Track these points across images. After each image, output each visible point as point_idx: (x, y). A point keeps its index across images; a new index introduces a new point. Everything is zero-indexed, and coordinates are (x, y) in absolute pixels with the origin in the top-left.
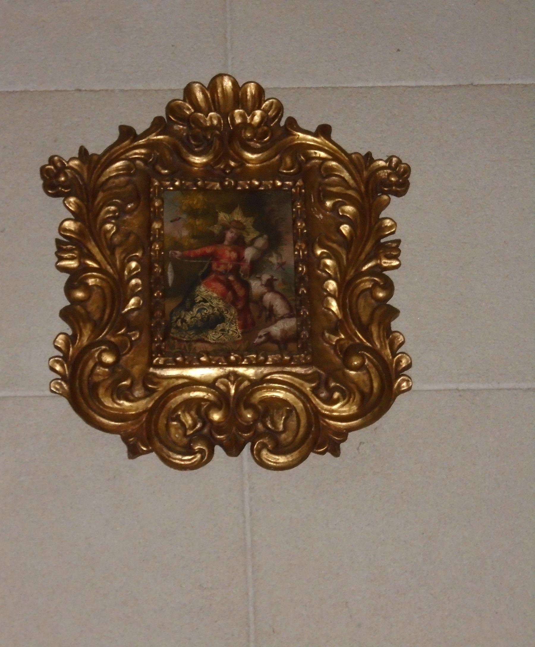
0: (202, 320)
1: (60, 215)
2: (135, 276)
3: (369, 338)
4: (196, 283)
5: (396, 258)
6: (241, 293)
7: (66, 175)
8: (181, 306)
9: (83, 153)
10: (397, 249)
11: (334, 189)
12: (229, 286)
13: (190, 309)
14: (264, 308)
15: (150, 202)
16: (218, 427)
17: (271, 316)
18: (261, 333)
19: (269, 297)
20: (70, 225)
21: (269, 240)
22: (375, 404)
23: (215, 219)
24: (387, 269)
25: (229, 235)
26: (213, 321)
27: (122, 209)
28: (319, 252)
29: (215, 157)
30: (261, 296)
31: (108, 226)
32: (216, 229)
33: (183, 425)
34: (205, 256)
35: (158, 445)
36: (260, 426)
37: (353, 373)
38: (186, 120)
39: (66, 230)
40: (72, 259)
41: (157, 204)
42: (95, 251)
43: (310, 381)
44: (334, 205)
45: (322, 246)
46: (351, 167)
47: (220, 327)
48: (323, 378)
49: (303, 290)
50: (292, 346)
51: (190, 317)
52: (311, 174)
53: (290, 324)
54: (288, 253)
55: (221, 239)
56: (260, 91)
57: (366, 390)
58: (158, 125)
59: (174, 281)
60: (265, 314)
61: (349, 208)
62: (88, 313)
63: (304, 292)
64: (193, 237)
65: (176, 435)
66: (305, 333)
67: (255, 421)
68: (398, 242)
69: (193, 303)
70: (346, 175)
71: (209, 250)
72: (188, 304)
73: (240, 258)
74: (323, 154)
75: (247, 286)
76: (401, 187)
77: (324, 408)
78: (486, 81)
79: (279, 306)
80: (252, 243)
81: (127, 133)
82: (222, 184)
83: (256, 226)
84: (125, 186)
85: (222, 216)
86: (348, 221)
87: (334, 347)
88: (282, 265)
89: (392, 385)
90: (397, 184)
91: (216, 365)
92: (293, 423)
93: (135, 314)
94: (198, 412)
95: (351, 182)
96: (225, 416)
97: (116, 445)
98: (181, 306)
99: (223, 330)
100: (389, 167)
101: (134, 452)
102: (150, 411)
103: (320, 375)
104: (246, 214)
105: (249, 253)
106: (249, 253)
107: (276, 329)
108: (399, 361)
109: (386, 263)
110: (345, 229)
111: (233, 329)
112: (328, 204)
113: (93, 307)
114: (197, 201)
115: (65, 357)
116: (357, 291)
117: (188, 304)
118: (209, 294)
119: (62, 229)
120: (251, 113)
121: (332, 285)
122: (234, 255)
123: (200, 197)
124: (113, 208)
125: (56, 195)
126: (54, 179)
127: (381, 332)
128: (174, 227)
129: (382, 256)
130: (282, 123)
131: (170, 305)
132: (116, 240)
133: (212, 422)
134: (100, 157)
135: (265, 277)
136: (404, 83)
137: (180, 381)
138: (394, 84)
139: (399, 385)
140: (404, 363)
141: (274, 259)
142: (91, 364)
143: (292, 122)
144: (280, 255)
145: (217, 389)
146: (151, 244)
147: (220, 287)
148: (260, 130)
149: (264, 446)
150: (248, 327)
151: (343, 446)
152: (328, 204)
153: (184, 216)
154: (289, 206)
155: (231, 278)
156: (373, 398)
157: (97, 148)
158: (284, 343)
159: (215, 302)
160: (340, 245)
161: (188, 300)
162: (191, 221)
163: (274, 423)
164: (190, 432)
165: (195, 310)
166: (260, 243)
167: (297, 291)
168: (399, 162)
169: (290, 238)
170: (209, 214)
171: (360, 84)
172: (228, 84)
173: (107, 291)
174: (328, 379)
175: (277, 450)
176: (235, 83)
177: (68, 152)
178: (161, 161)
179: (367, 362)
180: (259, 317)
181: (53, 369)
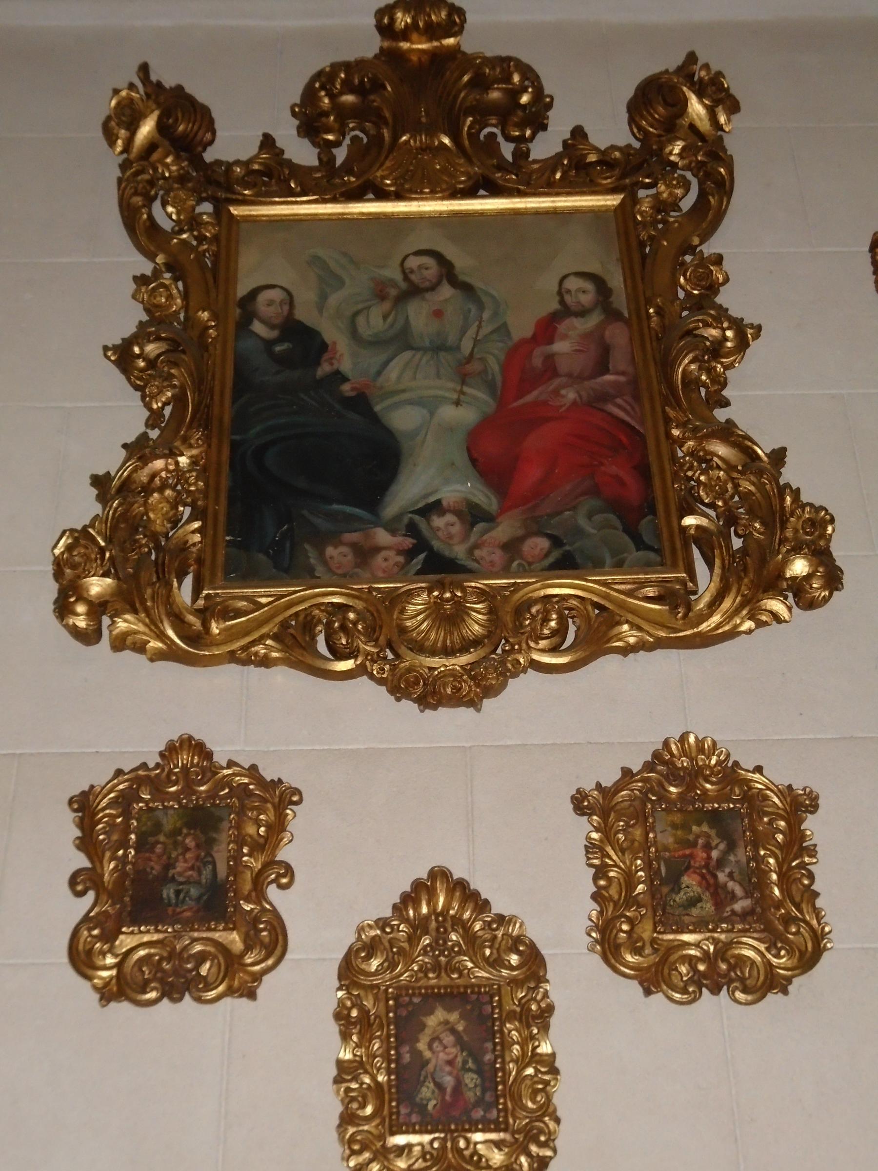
0: (687, 900)
1: (584, 829)
2: (641, 870)
3: (801, 912)
4: (681, 874)
5: (814, 856)
6: (712, 881)
7: (589, 801)
8: (672, 890)
9: (599, 786)
10: (814, 850)
11: (769, 810)
12: (703, 876)
13: (679, 892)
14: (728, 892)
15: (646, 819)
16: (703, 975)
17: (734, 898)
18: (728, 909)
19: (731, 884)
20: (595, 835)
21: (728, 845)
22: (808, 960)
23: (690, 831)
24: (808, 864)
25: (700, 841)
26: (694, 902)
27: (627, 824)
28: (762, 853)
29: (687, 788)
30: (726, 885)
31: (620, 836)
32: (691, 837)
33: (680, 974)
34: (685, 856)
35: (665, 987)
36: (732, 974)
37: (790, 936)
38: (664, 763)
39: (590, 838)
40: (597, 858)
41: (651, 820)
42: (612, 853)
43: (764, 943)
44: (770, 820)
45: (765, 849)
46: (779, 794)
47: (699, 905)
48: (773, 940)
49: (754, 880)
50: (749, 918)
51: (680, 897)
52: (754, 800)
53: (746, 903)
54: (741, 854)
55: (694, 845)
56: (714, 743)
57: (803, 949)
58: (649, 766)
59: (666, 873)
60: (729, 896)
61: (782, 823)
62: (610, 895)
63: (755, 881)
64: (678, 843)
65: (676, 980)
66: (759, 910)
67: (729, 970)
68: (815, 845)
69: (680, 889)
70: (776, 800)
71: (688, 852)
72: (676, 890)
73: (709, 857)
74: (760, 786)
75: (715, 877)
76: (814, 807)
77: (774, 961)
78: (860, 735)
79: (739, 891)
80: (716, 846)
81: (627, 773)
82: (693, 807)
83: (718, 835)
84: (628, 809)
85: (695, 828)
86: (781, 832)
87: (778, 919)
88: (737, 862)
89: (820, 945)
90: (811, 805)
91: (700, 932)
92: (755, 973)
93: (642, 896)
94: (690, 965)
95: (780, 804)
96: (708, 967)
97: (634, 988)
98: (672, 890)
99: (702, 907)
100: (805, 794)
101: (648, 992)
102: (657, 965)
103: (770, 939)
104: (711, 828)
105: (715, 854)
106: (715, 854)
107: (738, 906)
108: (823, 928)
109: (807, 859)
110: (780, 837)
111: (708, 907)
112: (766, 819)
113: (613, 892)
114: (677, 818)
115: (597, 926)
116: (791, 880)
117: (676, 890)
118: (690, 881)
119: (588, 838)
120: (709, 758)
121: (774, 877)
122: (705, 855)
123: (679, 815)
124: (622, 823)
125: (583, 814)
126: (580, 804)
127: (414, 196)
128: (664, 836)
129: (805, 855)
130: (730, 765)
131: (665, 890)
132: (624, 845)
133: (699, 971)
134: (610, 788)
135: (727, 870)
136: (806, 737)
137: (676, 943)
138: (800, 737)
139: (825, 945)
140: (827, 929)
141: (732, 858)
142: (615, 931)
143: (736, 763)
144: (736, 855)
145: (702, 948)
146: (649, 848)
147: (698, 878)
148: (715, 770)
149: (736, 988)
150: (719, 905)
151: (790, 988)
152: (766, 819)
153: (669, 829)
154: (739, 821)
155: (704, 871)
156: (808, 955)
157: (607, 783)
158: (744, 916)
159: (695, 888)
160: (776, 848)
161: (677, 888)
162: (674, 831)
163: (742, 972)
164: (685, 979)
165: (682, 893)
166: (722, 846)
167: (750, 880)
168: (811, 792)
169: (742, 844)
170: (685, 827)
171: (776, 737)
172: (692, 739)
173: (622, 881)
174: (774, 940)
175: (745, 991)
176: (696, 738)
177: (588, 786)
178: (651, 790)
179: (802, 929)
180: (726, 897)
181: (589, 935)
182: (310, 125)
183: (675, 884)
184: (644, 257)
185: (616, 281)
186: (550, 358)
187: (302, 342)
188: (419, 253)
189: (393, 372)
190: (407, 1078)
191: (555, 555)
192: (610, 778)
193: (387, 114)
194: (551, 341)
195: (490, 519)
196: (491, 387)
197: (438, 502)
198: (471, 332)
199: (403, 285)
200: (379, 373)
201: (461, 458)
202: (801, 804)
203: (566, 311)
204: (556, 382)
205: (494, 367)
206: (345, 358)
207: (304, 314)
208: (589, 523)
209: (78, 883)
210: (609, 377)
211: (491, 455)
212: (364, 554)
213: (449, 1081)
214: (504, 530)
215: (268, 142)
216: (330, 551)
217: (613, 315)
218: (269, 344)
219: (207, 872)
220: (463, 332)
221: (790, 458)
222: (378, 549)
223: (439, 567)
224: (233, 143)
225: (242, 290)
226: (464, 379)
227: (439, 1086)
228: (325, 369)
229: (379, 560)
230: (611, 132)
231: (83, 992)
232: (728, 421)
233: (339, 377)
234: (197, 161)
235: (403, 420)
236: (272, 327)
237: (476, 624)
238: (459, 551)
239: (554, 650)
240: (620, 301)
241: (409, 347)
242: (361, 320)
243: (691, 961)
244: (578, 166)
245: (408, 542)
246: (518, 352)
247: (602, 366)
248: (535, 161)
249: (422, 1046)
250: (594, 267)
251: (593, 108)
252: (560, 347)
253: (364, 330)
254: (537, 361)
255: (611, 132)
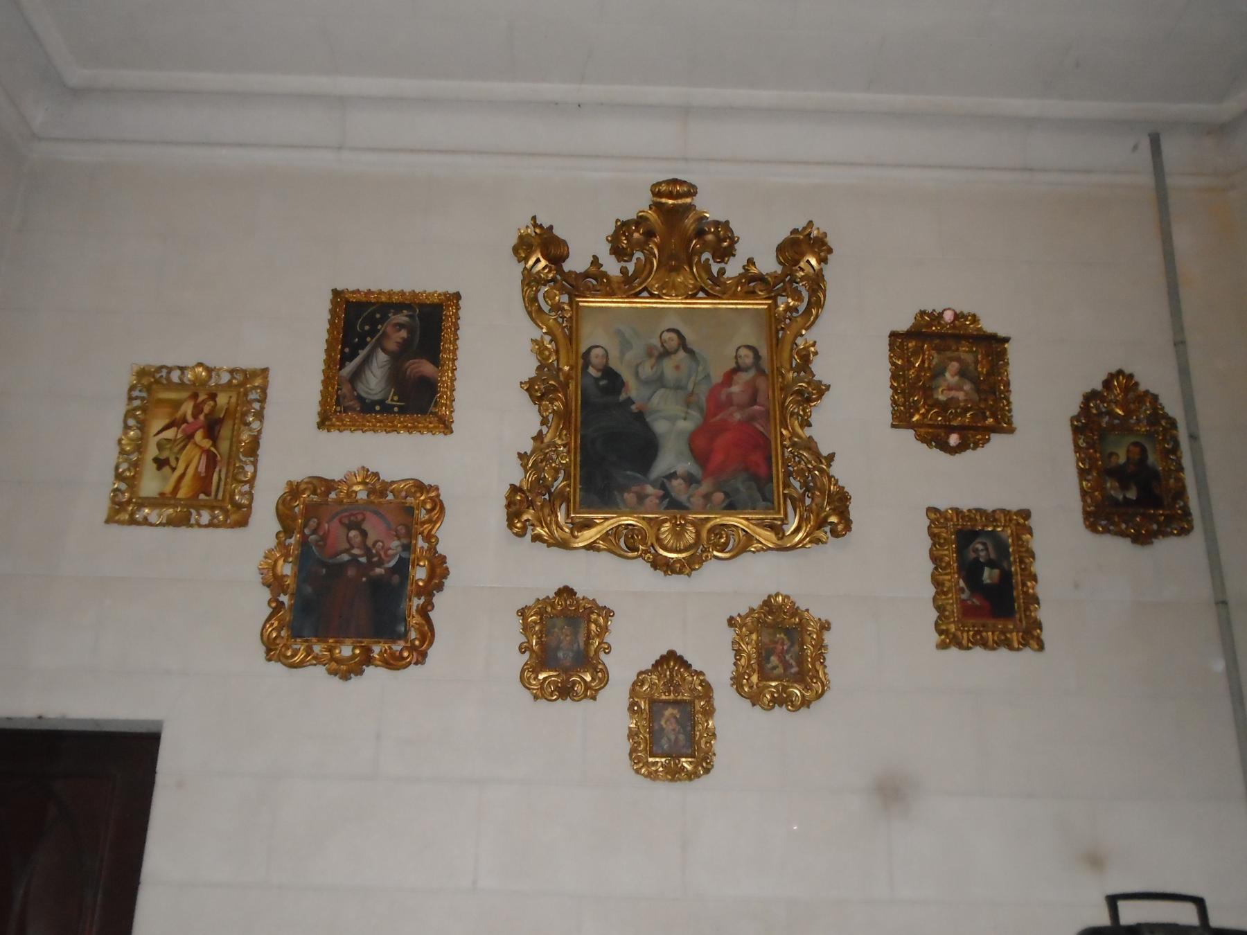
1: (731, 634)
17: (791, 666)
26: (775, 668)
51: (769, 666)
54: (796, 648)
58: (761, 607)
63: (801, 661)
76: (828, 629)
111: (780, 670)
174: (807, 687)
182: (618, 252)
183: (768, 659)
184: (778, 339)
185: (764, 352)
186: (730, 396)
187: (612, 379)
188: (669, 330)
189: (656, 400)
190: (655, 735)
191: (727, 501)
192: (744, 612)
193: (656, 251)
194: (730, 385)
195: (698, 482)
196: (701, 410)
197: (675, 473)
198: (693, 379)
199: (661, 350)
200: (649, 399)
201: (687, 451)
202: (825, 626)
203: (738, 369)
204: (732, 409)
205: (703, 399)
206: (633, 390)
207: (614, 364)
208: (741, 485)
209: (522, 650)
210: (756, 407)
211: (699, 447)
212: (641, 498)
213: (673, 737)
214: (705, 488)
215: (595, 261)
216: (626, 495)
217: (761, 372)
218: (597, 380)
219: (576, 646)
220: (690, 376)
221: (836, 458)
222: (647, 496)
223: (674, 504)
224: (576, 263)
225: (583, 349)
226: (688, 404)
227: (669, 740)
228: (623, 397)
229: (648, 501)
230: (768, 265)
231: (527, 695)
232: (810, 438)
233: (630, 401)
234: (560, 270)
235: (660, 427)
236: (598, 370)
237: (690, 537)
238: (683, 498)
239: (722, 551)
240: (765, 364)
241: (663, 386)
242: (640, 370)
243: (772, 693)
244: (752, 282)
245: (661, 493)
246: (714, 392)
247: (753, 400)
248: (729, 279)
249: (663, 723)
250: (752, 342)
251: (758, 248)
252: (735, 389)
253: (643, 376)
254: (723, 397)
255: (768, 265)
